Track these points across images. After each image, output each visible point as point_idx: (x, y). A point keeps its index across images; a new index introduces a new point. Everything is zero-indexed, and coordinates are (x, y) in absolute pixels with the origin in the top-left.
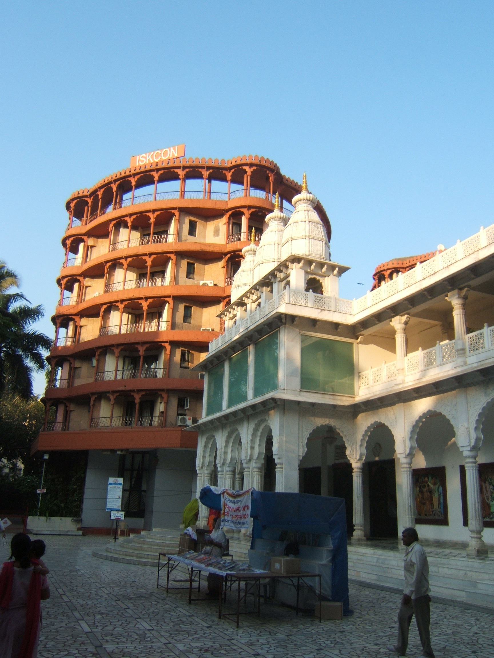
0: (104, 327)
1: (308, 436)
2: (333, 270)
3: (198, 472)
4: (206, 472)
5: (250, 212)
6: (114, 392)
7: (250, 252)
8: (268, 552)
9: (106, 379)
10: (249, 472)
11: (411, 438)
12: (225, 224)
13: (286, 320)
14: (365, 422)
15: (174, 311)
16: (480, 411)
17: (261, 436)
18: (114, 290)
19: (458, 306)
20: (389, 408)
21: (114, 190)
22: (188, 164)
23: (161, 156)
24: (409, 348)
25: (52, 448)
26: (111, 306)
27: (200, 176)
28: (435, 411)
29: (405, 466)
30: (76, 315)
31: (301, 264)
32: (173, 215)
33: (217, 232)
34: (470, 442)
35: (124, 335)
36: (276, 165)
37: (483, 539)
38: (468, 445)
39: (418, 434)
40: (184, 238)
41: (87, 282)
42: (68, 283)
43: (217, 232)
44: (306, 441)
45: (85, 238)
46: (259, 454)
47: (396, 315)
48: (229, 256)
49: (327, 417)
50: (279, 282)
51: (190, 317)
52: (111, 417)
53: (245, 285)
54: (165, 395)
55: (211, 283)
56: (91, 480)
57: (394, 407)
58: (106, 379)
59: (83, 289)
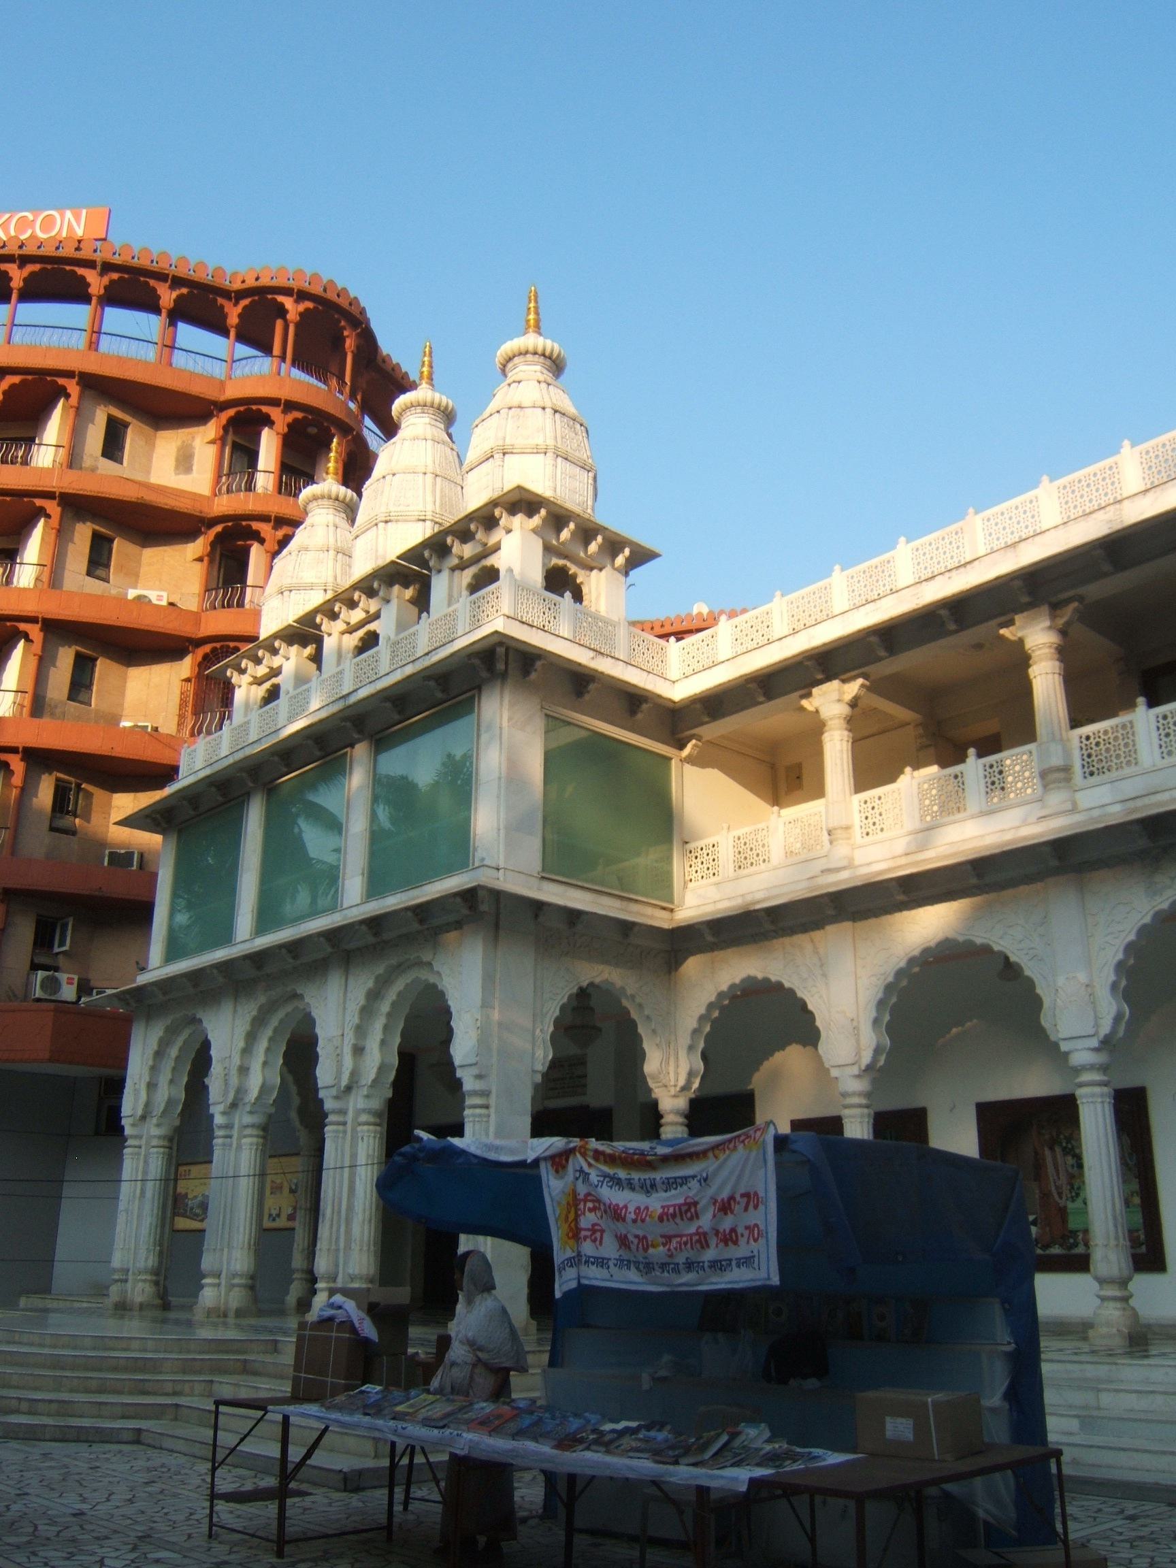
1: (557, 1013)
2: (614, 556)
3: (128, 1131)
4: (155, 1131)
5: (290, 418)
7: (326, 502)
8: (663, 1373)
10: (344, 1124)
12: (212, 442)
13: (506, 664)
14: (709, 980)
15: (44, 663)
16: (1132, 937)
17: (389, 1015)
19: (1047, 650)
20: (800, 939)
22: (117, 259)
23: (33, 227)
24: (872, 771)
27: (150, 305)
28: (969, 944)
31: (536, 520)
32: (63, 392)
33: (185, 462)
34: (1097, 1025)
36: (363, 311)
37: (1132, 1302)
38: (1092, 1032)
39: (708, 1039)
40: (87, 462)
43: (185, 462)
44: (551, 1029)
46: (382, 1069)
47: (828, 679)
48: (219, 528)
49: (607, 963)
50: (453, 569)
51: (89, 687)
53: (311, 587)
55: (160, 598)
57: (817, 935)
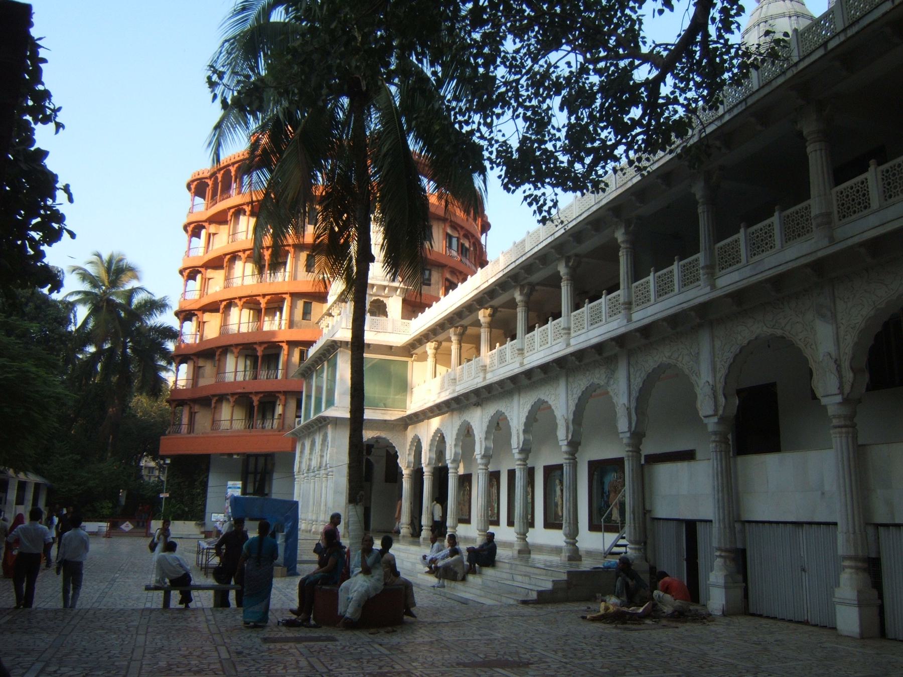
0: (224, 324)
6: (233, 394)
9: (227, 380)
11: (430, 450)
18: (235, 285)
21: (233, 173)
25: (173, 453)
26: (230, 303)
29: (481, 467)
30: (199, 310)
35: (244, 334)
41: (210, 273)
42: (191, 273)
45: (206, 224)
49: (379, 430)
52: (231, 420)
54: (282, 397)
56: (213, 481)
58: (227, 380)
59: (206, 281)
